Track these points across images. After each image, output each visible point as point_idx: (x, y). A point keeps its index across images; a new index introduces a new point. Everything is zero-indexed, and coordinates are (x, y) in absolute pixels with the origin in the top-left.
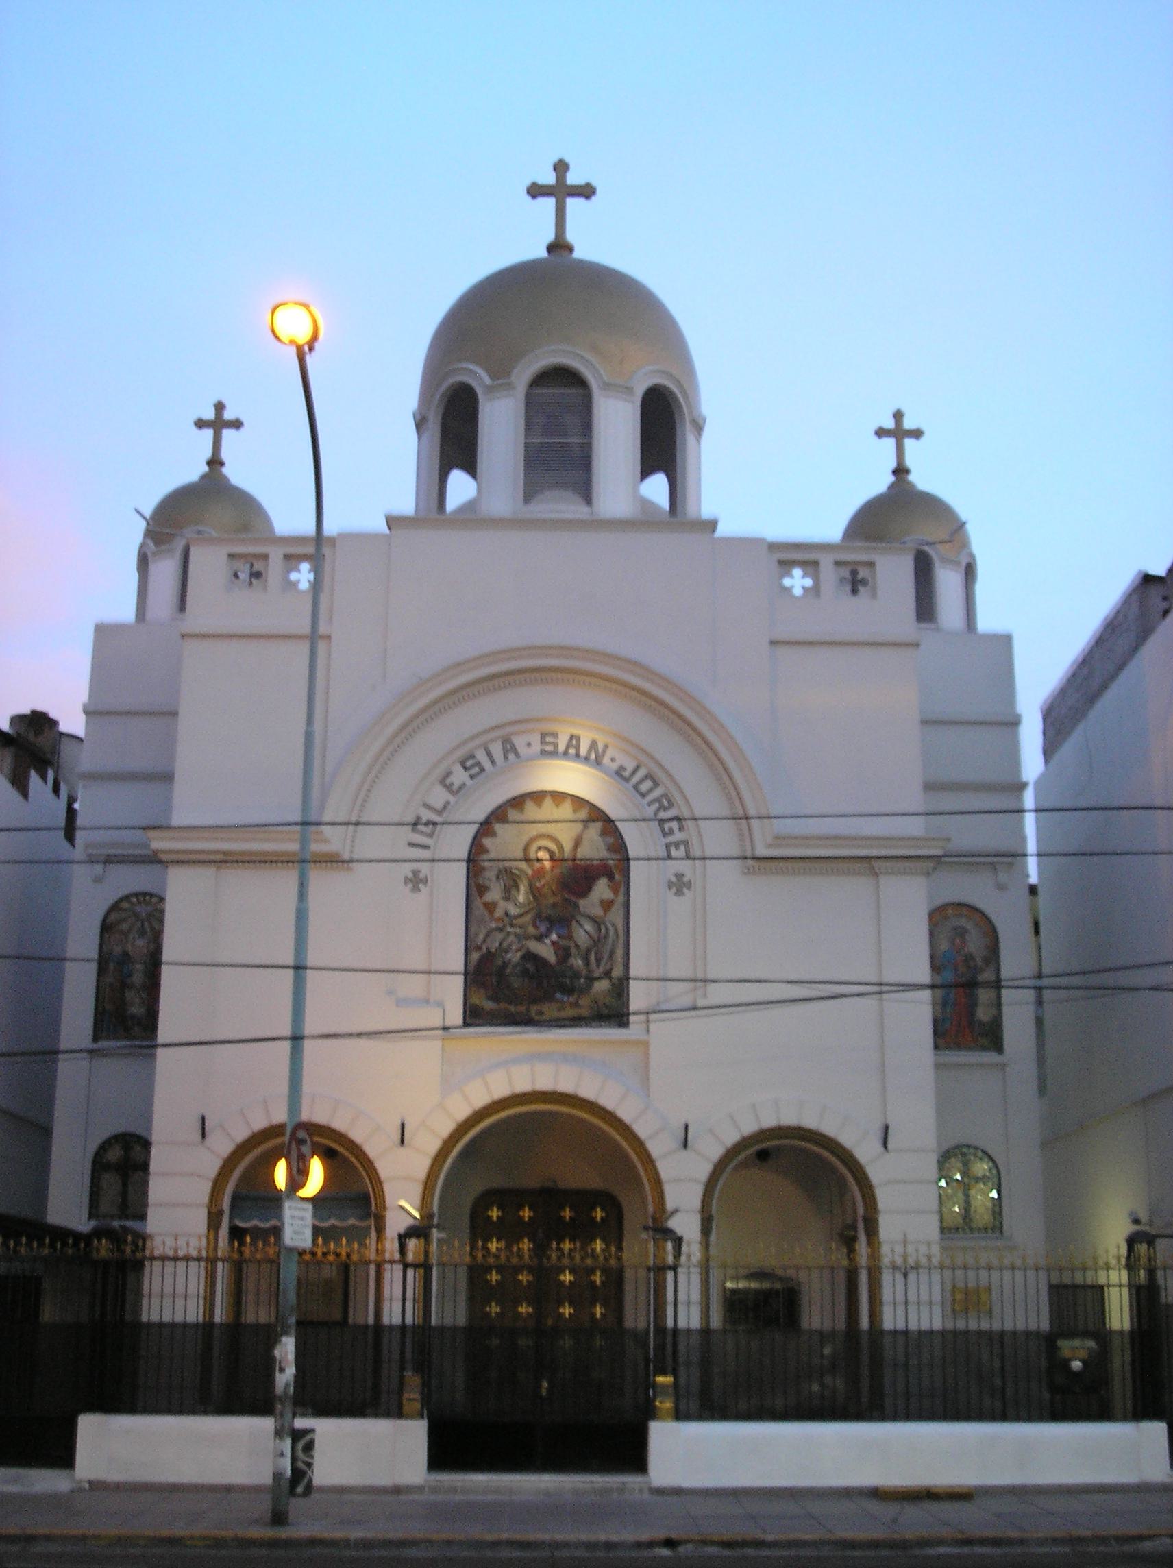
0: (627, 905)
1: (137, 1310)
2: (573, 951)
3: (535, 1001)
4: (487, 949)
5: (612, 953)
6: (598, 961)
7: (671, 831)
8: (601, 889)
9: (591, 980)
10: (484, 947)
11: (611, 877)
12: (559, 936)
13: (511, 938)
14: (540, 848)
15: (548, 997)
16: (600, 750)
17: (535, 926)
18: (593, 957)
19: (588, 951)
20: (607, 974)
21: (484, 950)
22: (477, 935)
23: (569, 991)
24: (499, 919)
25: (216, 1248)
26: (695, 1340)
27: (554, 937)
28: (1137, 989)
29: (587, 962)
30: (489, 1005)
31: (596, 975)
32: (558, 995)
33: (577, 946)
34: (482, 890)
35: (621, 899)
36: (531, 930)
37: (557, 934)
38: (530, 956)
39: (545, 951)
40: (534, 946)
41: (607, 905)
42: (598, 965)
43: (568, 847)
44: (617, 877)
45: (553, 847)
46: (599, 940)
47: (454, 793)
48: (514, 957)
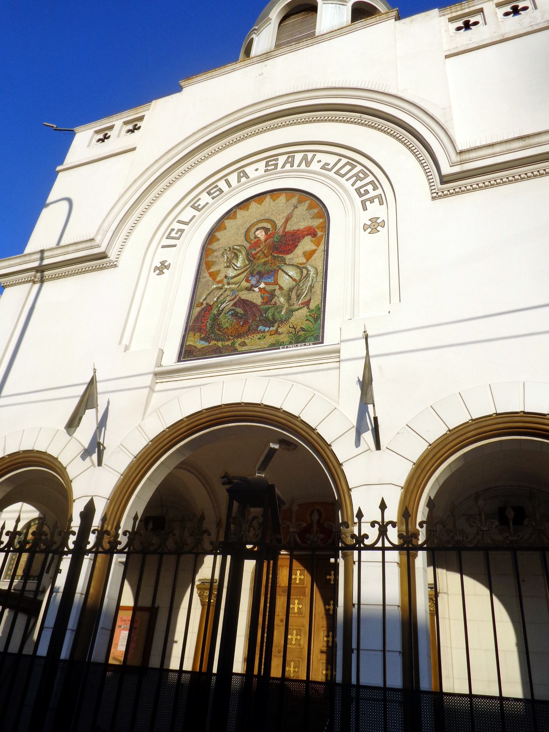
0: (327, 251)
1: (169, 664)
2: (277, 292)
3: (239, 336)
4: (207, 304)
5: (311, 287)
6: (298, 296)
7: (367, 192)
8: (306, 244)
9: (290, 312)
10: (205, 303)
11: (314, 235)
12: (266, 284)
13: (228, 292)
14: (257, 229)
15: (251, 331)
16: (304, 161)
17: (247, 281)
18: (294, 295)
19: (291, 290)
20: (307, 304)
21: (204, 305)
22: (202, 294)
23: (270, 323)
24: (220, 282)
25: (53, 558)
26: (321, 688)
27: (262, 285)
28: (5, 446)
29: (289, 299)
30: (200, 344)
31: (296, 307)
32: (261, 328)
33: (281, 288)
34: (209, 265)
35: (322, 247)
36: (244, 284)
37: (264, 283)
38: (244, 303)
39: (255, 297)
40: (245, 295)
41: (309, 255)
42: (298, 300)
43: (280, 223)
44: (319, 234)
45: (269, 226)
46: (300, 281)
47: (199, 210)
48: (227, 305)
